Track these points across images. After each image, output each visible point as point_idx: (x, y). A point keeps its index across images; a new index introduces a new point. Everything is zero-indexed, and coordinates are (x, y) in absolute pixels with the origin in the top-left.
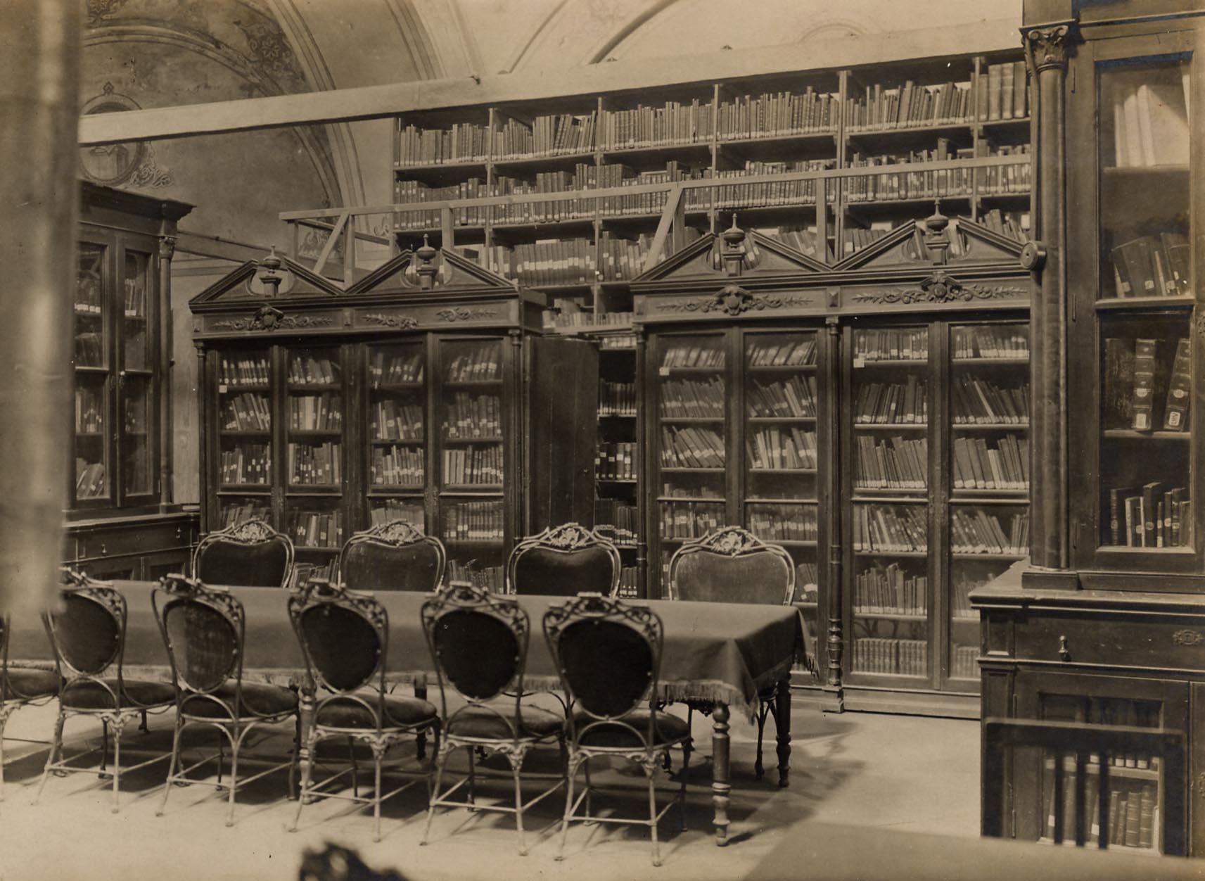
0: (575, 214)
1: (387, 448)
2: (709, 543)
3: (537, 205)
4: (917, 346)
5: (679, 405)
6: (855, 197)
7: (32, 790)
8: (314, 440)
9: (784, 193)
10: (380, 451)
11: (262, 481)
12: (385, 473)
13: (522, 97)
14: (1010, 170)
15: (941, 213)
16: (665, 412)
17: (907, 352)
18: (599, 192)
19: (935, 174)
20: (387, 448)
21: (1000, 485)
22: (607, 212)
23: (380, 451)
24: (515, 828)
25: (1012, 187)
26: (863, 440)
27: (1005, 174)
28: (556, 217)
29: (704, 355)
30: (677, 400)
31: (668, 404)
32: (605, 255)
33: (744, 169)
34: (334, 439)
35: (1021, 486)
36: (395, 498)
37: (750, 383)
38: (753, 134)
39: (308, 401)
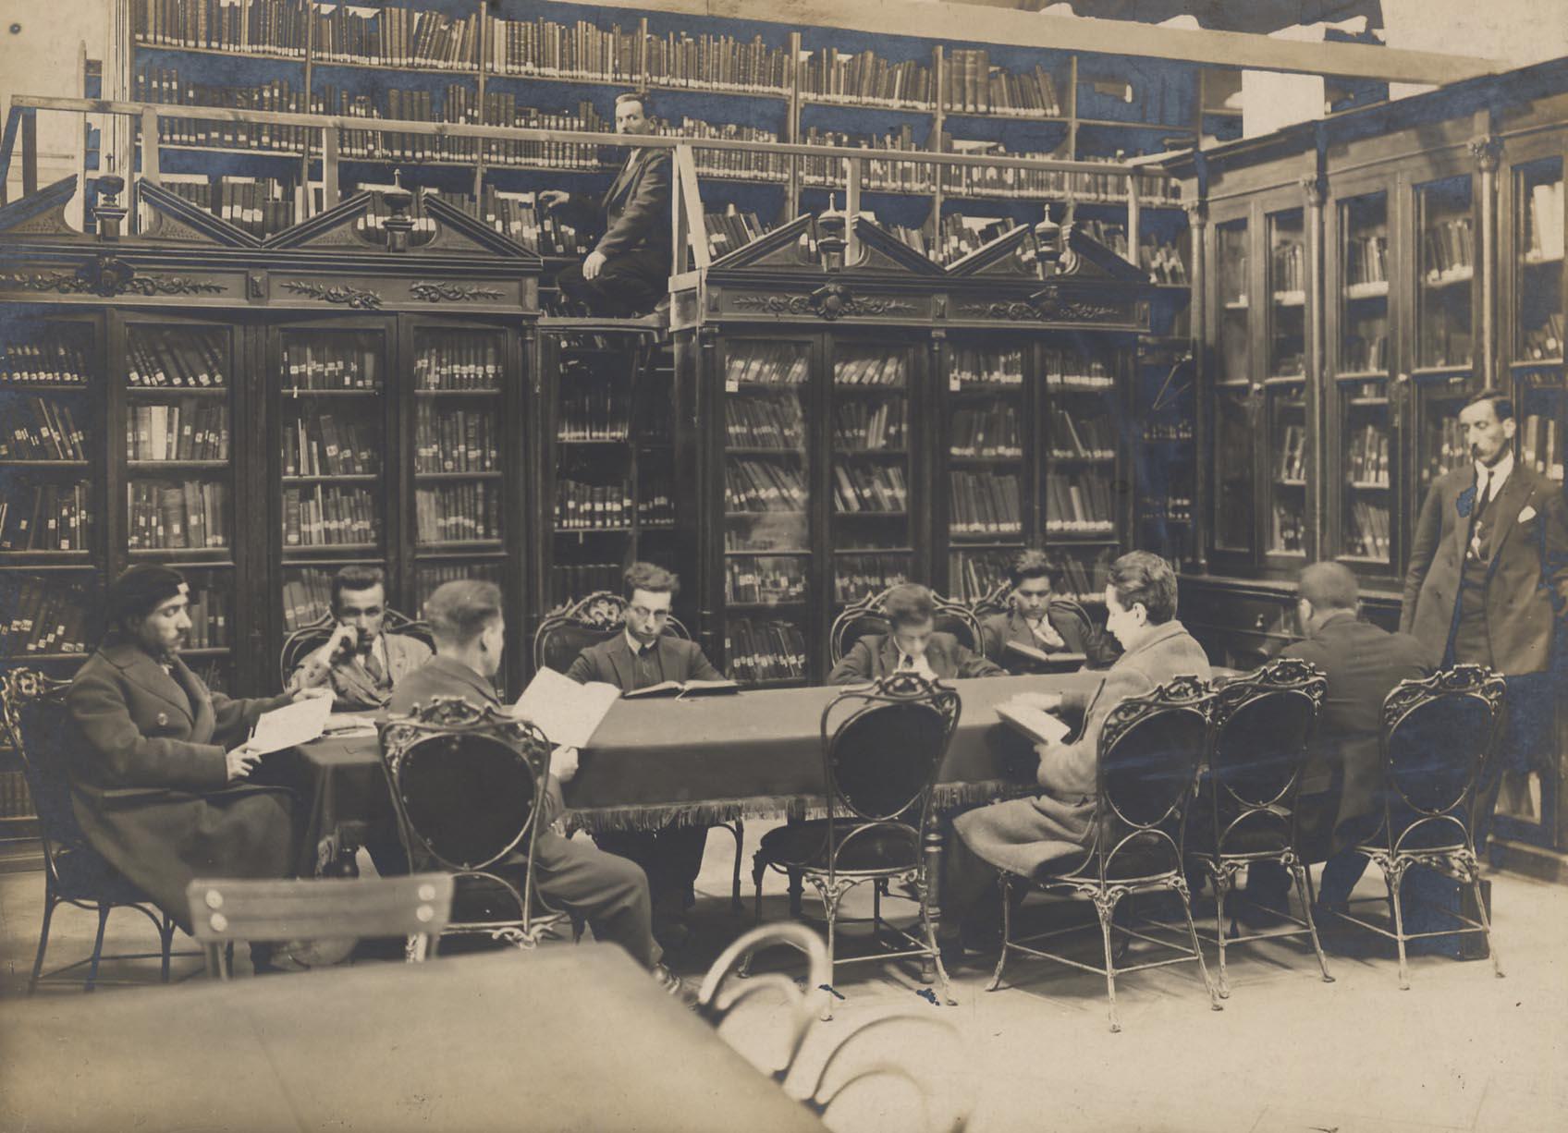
0: (445, 155)
1: (306, 491)
2: (875, 606)
3: (388, 136)
4: (1008, 370)
5: (745, 430)
6: (812, 179)
7: (1141, 1008)
8: (169, 475)
9: (728, 163)
10: (296, 493)
11: (65, 544)
12: (304, 528)
13: (872, 29)
14: (975, 171)
15: (1052, 220)
16: (726, 438)
17: (996, 375)
18: (485, 130)
19: (900, 165)
20: (306, 491)
21: (1081, 525)
22: (494, 158)
23: (296, 493)
24: (1105, 992)
25: (976, 190)
26: (956, 476)
27: (969, 175)
28: (419, 155)
29: (767, 368)
30: (742, 424)
31: (731, 430)
32: (491, 218)
33: (681, 126)
34: (205, 475)
35: (1105, 525)
36: (315, 566)
37: (829, 405)
38: (224, 47)
39: (158, 414)
